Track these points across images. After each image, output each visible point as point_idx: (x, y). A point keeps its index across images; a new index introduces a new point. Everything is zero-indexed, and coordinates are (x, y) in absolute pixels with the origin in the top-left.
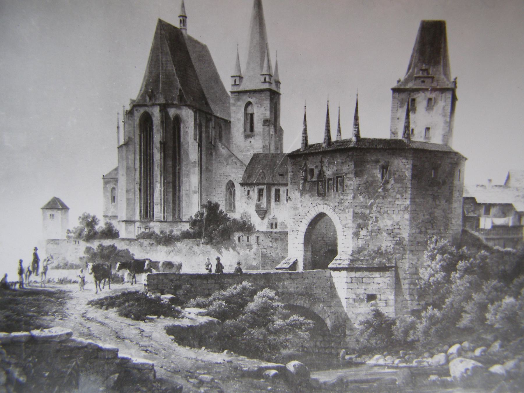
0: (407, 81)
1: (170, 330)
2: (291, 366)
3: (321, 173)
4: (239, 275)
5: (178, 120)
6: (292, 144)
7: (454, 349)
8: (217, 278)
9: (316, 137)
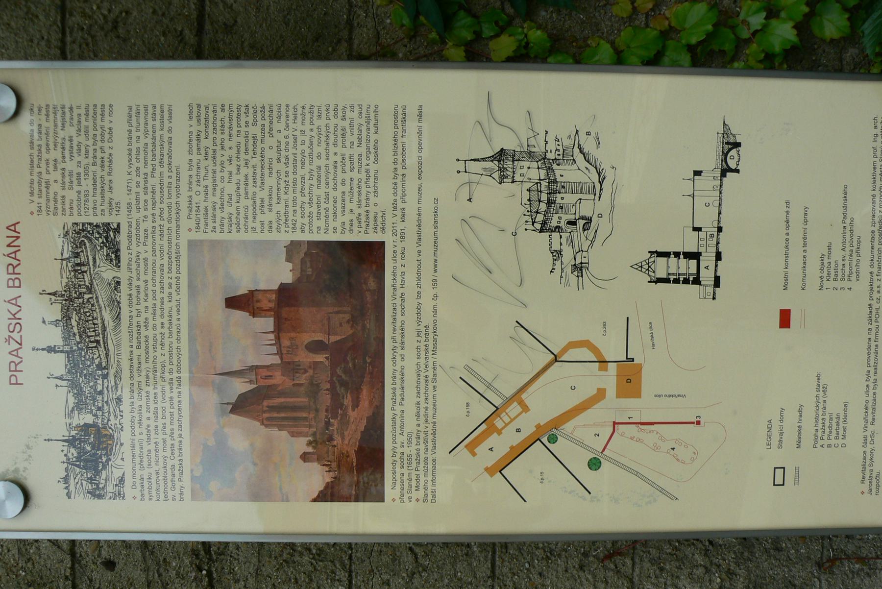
0: (249, 312)
1: (353, 410)
2: (368, 361)
3: (288, 347)
4: (332, 382)
5: (268, 407)
6: (276, 360)
7: (364, 286)
8: (333, 390)
9: (274, 349)
